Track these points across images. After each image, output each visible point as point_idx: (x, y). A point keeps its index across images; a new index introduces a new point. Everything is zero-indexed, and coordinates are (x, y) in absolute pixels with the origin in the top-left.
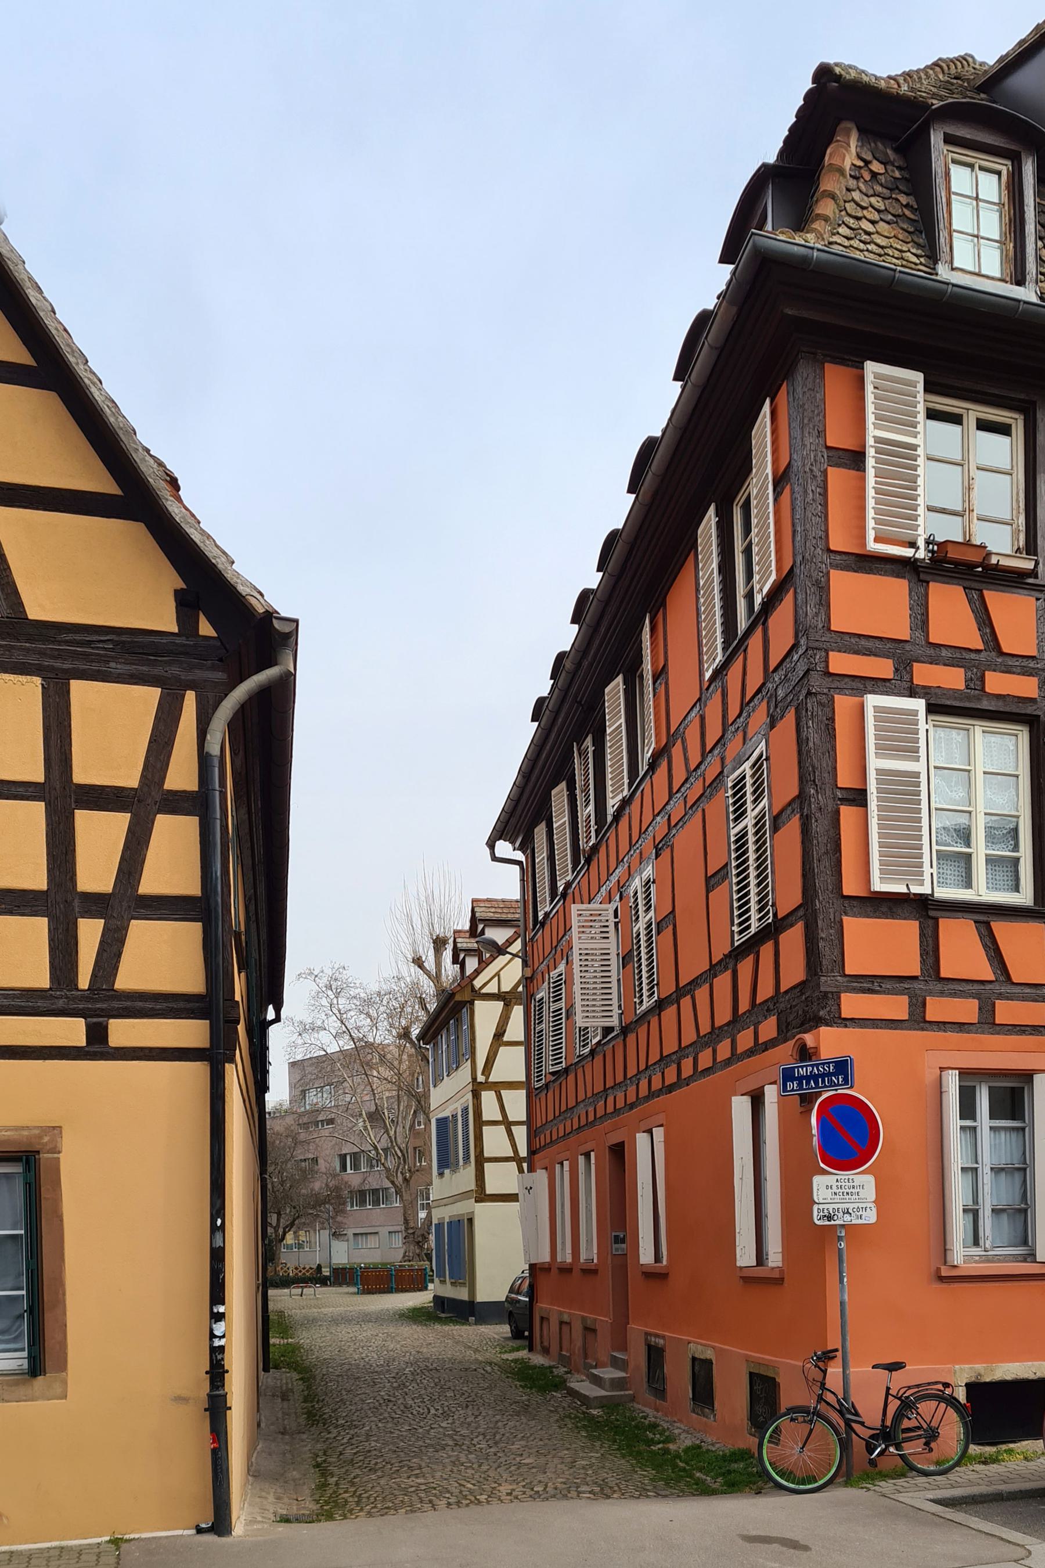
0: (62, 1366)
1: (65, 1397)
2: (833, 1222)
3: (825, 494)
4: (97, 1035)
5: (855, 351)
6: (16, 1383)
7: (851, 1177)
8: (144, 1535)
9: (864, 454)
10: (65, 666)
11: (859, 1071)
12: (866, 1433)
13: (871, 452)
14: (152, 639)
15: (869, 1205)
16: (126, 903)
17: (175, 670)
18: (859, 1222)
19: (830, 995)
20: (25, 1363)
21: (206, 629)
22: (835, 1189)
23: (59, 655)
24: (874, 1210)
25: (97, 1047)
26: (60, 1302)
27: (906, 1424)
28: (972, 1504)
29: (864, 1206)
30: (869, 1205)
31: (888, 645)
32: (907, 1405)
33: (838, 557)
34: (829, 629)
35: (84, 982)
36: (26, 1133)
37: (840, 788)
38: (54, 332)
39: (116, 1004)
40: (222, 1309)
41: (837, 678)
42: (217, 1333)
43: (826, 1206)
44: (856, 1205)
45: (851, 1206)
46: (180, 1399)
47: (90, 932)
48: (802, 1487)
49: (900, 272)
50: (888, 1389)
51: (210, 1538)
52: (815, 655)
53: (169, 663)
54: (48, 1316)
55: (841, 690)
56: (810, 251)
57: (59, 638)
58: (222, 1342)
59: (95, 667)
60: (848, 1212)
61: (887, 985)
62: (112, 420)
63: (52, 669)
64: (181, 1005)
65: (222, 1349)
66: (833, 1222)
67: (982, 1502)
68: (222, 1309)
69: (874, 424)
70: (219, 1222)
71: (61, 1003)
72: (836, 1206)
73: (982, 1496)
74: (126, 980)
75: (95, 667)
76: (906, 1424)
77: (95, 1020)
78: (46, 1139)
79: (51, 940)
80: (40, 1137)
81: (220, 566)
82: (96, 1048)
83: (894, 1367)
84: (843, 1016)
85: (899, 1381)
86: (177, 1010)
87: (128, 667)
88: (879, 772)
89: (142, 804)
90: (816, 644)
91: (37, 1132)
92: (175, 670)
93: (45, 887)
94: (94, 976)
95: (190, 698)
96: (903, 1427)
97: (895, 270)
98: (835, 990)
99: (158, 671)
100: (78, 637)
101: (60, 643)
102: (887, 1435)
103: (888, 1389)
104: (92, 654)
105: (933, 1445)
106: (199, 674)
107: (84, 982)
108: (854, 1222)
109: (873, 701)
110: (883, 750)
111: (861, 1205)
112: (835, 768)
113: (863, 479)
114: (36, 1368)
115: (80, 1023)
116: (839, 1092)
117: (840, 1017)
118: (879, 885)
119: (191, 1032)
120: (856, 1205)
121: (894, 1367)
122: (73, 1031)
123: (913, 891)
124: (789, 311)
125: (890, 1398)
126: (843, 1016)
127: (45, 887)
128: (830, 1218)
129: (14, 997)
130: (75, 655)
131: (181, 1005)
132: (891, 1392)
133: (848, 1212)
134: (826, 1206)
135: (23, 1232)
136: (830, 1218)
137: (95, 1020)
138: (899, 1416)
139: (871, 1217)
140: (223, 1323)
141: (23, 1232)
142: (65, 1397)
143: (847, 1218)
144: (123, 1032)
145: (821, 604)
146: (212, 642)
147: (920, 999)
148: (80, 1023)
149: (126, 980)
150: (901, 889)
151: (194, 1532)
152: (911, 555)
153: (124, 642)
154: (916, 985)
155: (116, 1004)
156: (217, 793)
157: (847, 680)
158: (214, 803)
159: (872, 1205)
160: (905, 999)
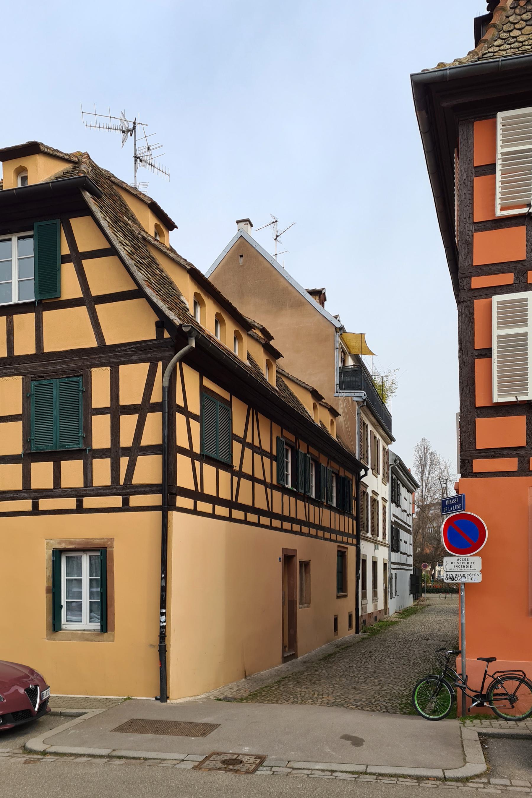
0: (113, 630)
1: (114, 641)
2: (455, 582)
3: (472, 194)
4: (126, 502)
5: (488, 111)
6: (98, 635)
7: (466, 558)
8: (138, 698)
9: (495, 164)
10: (118, 361)
11: (468, 502)
12: (473, 694)
13: (499, 162)
14: (147, 343)
15: (477, 573)
16: (137, 450)
17: (155, 354)
18: (471, 581)
19: (467, 461)
20: (99, 628)
21: (167, 335)
22: (456, 564)
23: (116, 357)
24: (480, 575)
25: (126, 507)
26: (113, 605)
27: (496, 691)
28: (510, 738)
29: (474, 573)
30: (477, 573)
31: (512, 265)
32: (497, 682)
33: (480, 225)
34: (472, 265)
35: (122, 482)
36: (103, 541)
37: (476, 350)
38: (109, 234)
39: (132, 490)
40: (164, 611)
41: (477, 291)
42: (162, 620)
43: (451, 573)
44: (469, 573)
45: (466, 573)
46: (152, 646)
47: (124, 462)
48: (431, 717)
49: (502, 61)
50: (486, 671)
51: (158, 702)
52: (463, 281)
53: (153, 352)
54: (109, 610)
55: (479, 297)
56: (445, 71)
57: (116, 350)
58: (164, 624)
59: (127, 359)
60: (464, 576)
61: (505, 453)
62: (127, 262)
63: (113, 363)
64: (155, 488)
65: (164, 627)
66: (455, 582)
67: (517, 739)
68: (164, 611)
69: (501, 146)
70: (163, 576)
71: (114, 491)
72: (457, 573)
73: (518, 735)
74: (136, 480)
75: (127, 359)
76: (496, 691)
77: (125, 496)
78: (109, 543)
79: (111, 467)
80: (107, 542)
81: (163, 310)
82: (125, 507)
83: (489, 660)
84: (474, 471)
85: (492, 668)
86: (154, 491)
87: (138, 357)
88: (499, 337)
89: (141, 410)
90: (464, 275)
91: (106, 540)
92: (155, 354)
93: (110, 447)
94: (125, 479)
95: (160, 364)
96: (494, 693)
97: (498, 61)
98: (470, 458)
99: (149, 356)
100: (122, 349)
101: (116, 352)
102: (483, 697)
103: (486, 671)
104: (126, 354)
105: (514, 704)
106: (164, 354)
107: (122, 482)
108: (467, 582)
109: (496, 299)
110: (502, 324)
111: (472, 573)
112: (474, 340)
113: (495, 178)
114: (104, 629)
115: (120, 498)
116: (461, 512)
117: (472, 472)
118: (497, 399)
119: (155, 499)
120: (469, 573)
121: (489, 660)
122: (117, 501)
123: (519, 400)
124: (445, 105)
125: (487, 676)
126: (474, 471)
127: (110, 447)
128: (453, 579)
129: (100, 489)
130: (121, 356)
131: (155, 488)
132: (487, 673)
133: (464, 576)
134: (451, 573)
135: (99, 578)
136: (453, 579)
137: (125, 496)
138: (493, 686)
139: (478, 579)
140: (164, 617)
141: (99, 578)
142: (114, 641)
143: (463, 579)
144: (135, 500)
145: (468, 253)
146: (169, 340)
147: (526, 459)
148: (120, 498)
149: (136, 480)
150: (513, 399)
151: (154, 699)
152: (526, 211)
153: (137, 347)
154: (524, 451)
155: (132, 490)
156: (167, 402)
157: (483, 290)
158: (165, 405)
159: (479, 573)
160: (516, 460)
